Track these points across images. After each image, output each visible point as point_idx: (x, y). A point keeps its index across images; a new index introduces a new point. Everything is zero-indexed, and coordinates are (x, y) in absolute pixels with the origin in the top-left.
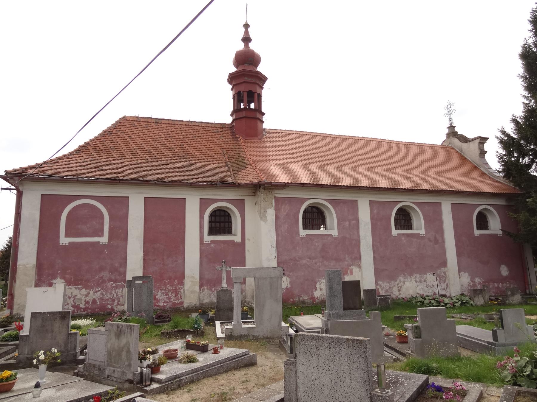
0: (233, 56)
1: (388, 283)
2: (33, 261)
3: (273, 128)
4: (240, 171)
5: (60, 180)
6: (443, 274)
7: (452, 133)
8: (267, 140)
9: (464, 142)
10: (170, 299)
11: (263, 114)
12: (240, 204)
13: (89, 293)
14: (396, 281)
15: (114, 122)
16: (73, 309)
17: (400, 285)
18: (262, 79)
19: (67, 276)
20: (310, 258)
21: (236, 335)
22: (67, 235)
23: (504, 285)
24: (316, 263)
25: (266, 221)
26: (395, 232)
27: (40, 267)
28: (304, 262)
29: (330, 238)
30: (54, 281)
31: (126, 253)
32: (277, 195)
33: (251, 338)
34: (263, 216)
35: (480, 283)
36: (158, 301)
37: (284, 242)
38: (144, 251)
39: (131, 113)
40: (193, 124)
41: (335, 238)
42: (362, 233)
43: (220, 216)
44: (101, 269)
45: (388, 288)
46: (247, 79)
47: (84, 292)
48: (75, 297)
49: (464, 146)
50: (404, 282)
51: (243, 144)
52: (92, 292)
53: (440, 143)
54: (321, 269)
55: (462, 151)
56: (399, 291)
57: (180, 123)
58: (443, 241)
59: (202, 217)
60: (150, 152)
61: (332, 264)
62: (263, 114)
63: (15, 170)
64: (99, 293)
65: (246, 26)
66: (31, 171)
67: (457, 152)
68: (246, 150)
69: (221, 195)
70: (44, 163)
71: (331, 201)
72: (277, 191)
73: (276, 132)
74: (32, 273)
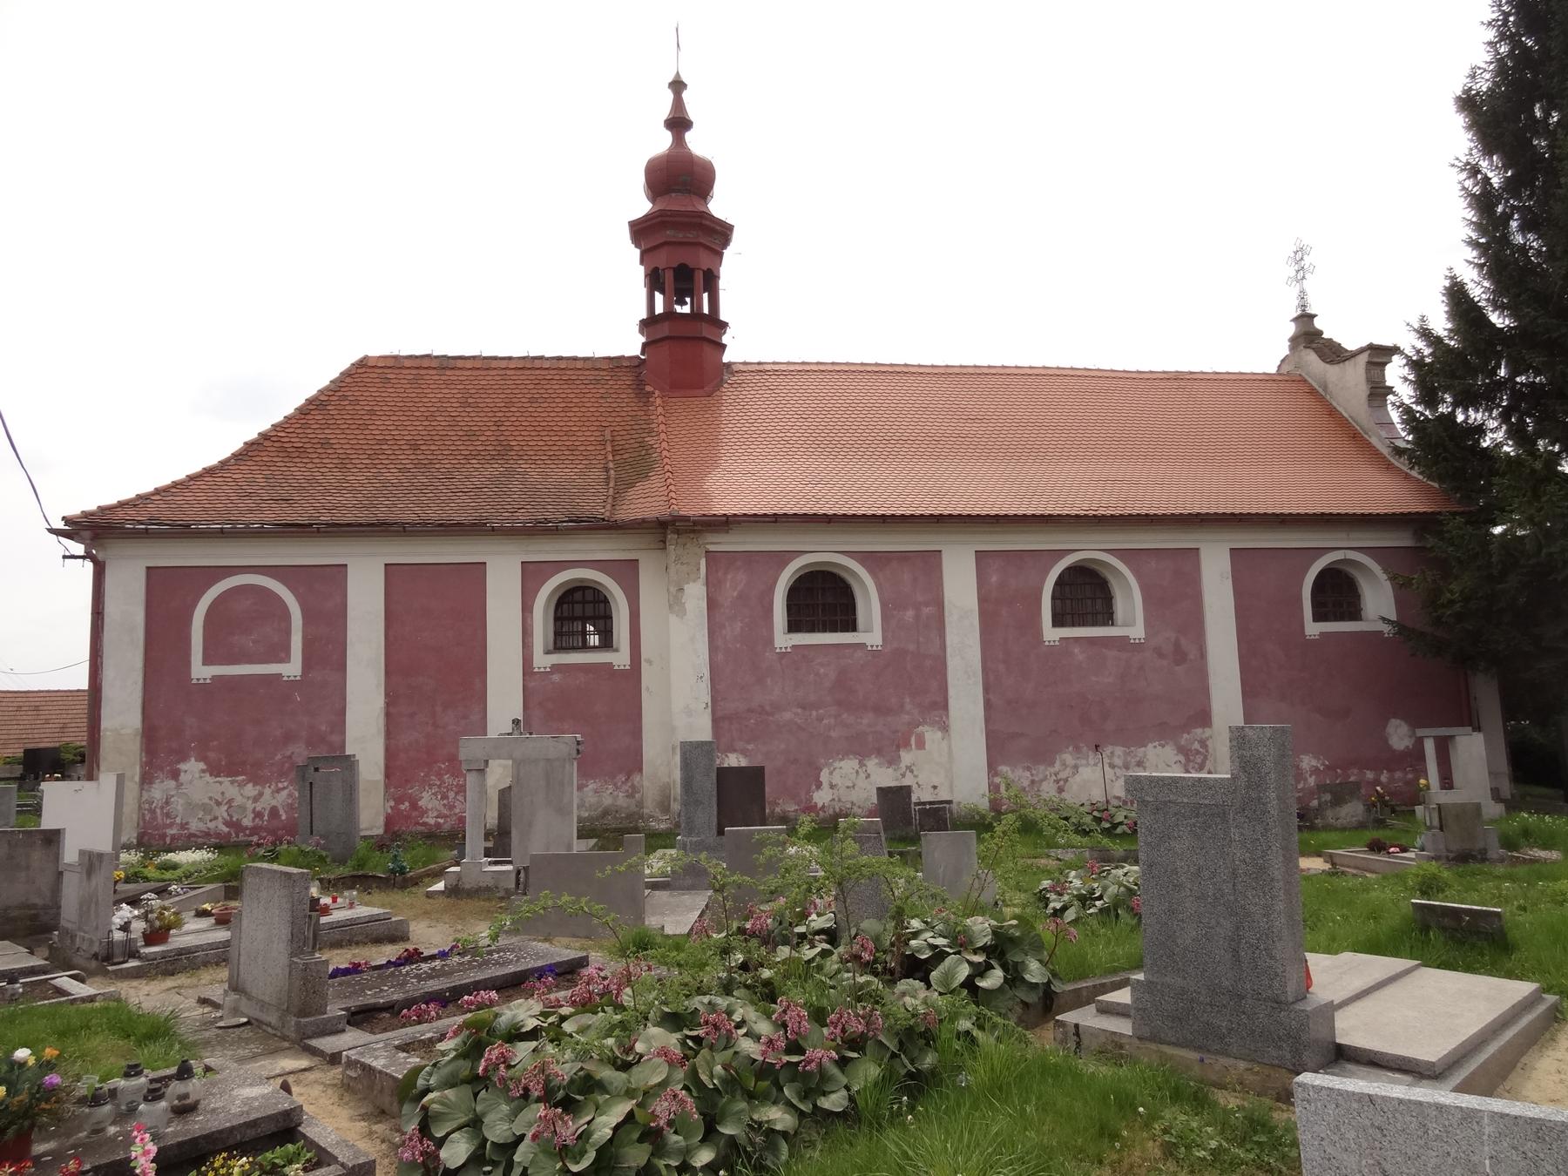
0: (640, 180)
1: (1028, 769)
2: (134, 720)
3: (753, 358)
4: (632, 485)
5: (183, 532)
6: (1196, 746)
7: (1307, 335)
8: (728, 394)
9: (1331, 362)
10: (452, 807)
11: (724, 325)
12: (627, 572)
13: (261, 794)
14: (1052, 764)
15: (335, 375)
16: (226, 830)
17: (1062, 775)
18: (721, 233)
19: (212, 755)
20: (804, 708)
21: (467, 886)
22: (207, 661)
23: (1398, 774)
24: (820, 719)
25: (682, 613)
26: (1052, 634)
27: (150, 735)
28: (787, 716)
29: (859, 654)
30: (182, 766)
31: (345, 699)
32: (712, 548)
33: (502, 894)
34: (676, 603)
35: (1315, 771)
36: (424, 812)
37: (734, 663)
38: (387, 695)
39: (378, 348)
40: (537, 364)
41: (875, 654)
42: (952, 638)
43: (584, 602)
44: (288, 738)
45: (1026, 783)
46: (680, 231)
47: (250, 790)
48: (230, 801)
49: (1332, 372)
50: (1076, 767)
51: (660, 410)
52: (267, 791)
53: (1273, 370)
54: (833, 734)
55: (1325, 388)
56: (1061, 790)
57: (503, 364)
58: (1202, 655)
59: (527, 608)
60: (415, 447)
61: (865, 721)
62: (724, 325)
63: (85, 514)
64: (285, 793)
65: (678, 86)
66: (120, 514)
67: (1313, 392)
68: (662, 427)
69: (574, 551)
70: (157, 491)
71: (865, 558)
72: (710, 538)
73: (760, 370)
74: (134, 747)
